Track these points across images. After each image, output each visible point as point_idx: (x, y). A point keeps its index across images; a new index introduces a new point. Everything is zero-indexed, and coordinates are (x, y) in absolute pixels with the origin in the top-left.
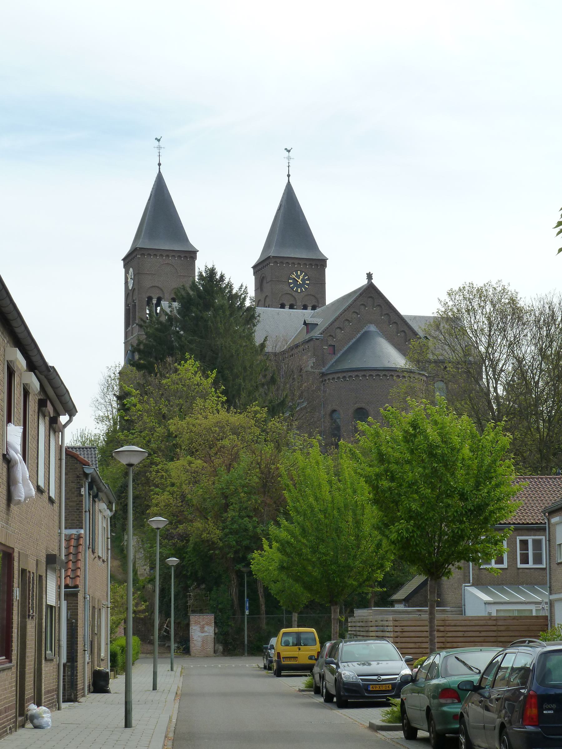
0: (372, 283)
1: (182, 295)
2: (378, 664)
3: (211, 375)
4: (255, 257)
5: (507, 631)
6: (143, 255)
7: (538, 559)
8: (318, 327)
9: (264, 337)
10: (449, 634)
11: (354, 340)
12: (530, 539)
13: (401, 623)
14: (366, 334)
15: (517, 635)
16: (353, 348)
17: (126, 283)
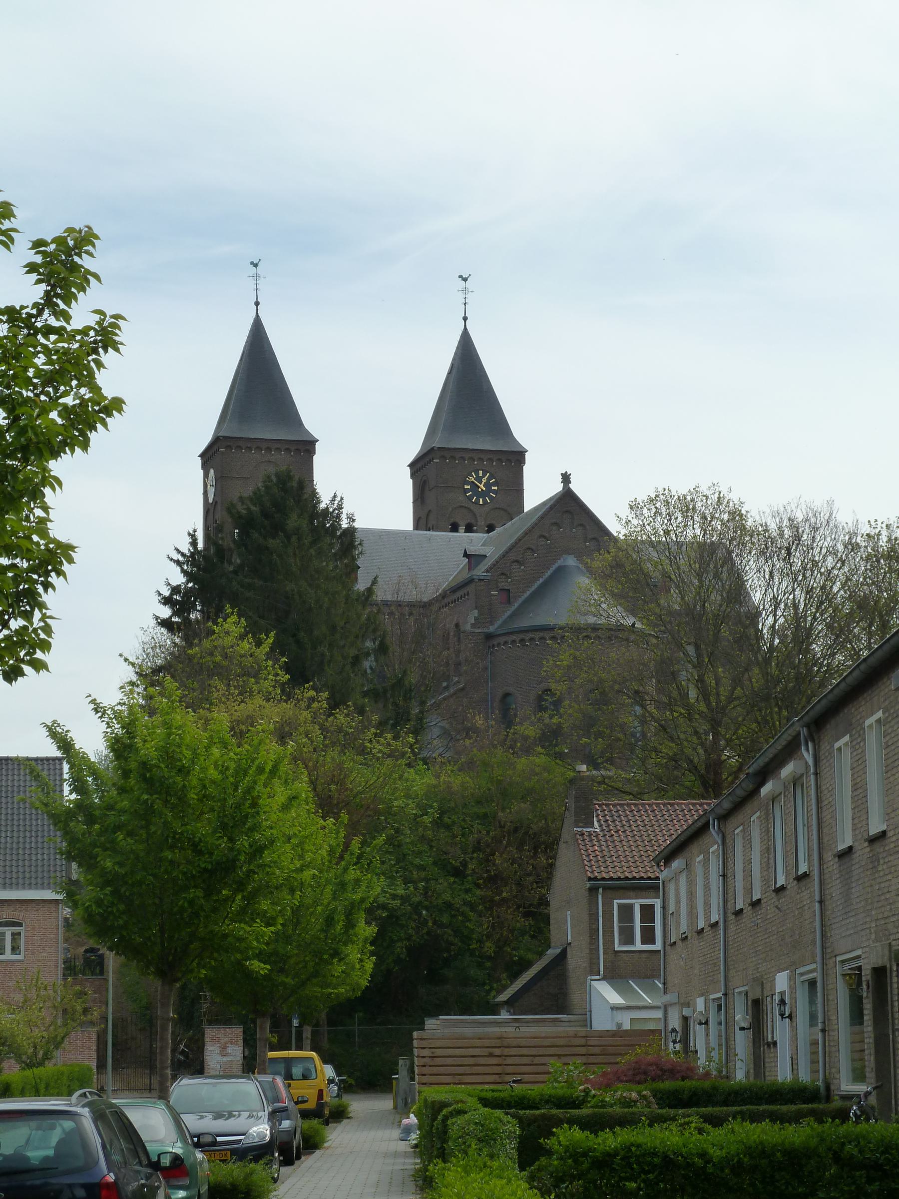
0: (569, 488)
1: (238, 513)
2: (202, 1117)
3: (266, 640)
4: (414, 449)
5: (603, 1055)
6: (229, 447)
7: (648, 936)
8: (487, 560)
9: (372, 578)
10: (509, 1061)
11: (541, 580)
12: (637, 904)
13: (430, 1043)
14: (561, 570)
15: (434, 1068)
16: (539, 594)
17: (205, 493)
